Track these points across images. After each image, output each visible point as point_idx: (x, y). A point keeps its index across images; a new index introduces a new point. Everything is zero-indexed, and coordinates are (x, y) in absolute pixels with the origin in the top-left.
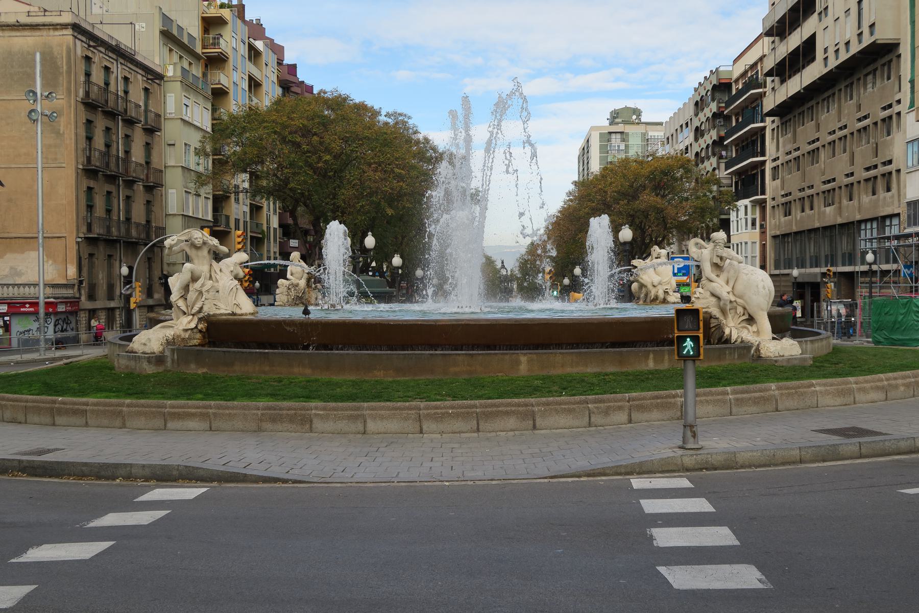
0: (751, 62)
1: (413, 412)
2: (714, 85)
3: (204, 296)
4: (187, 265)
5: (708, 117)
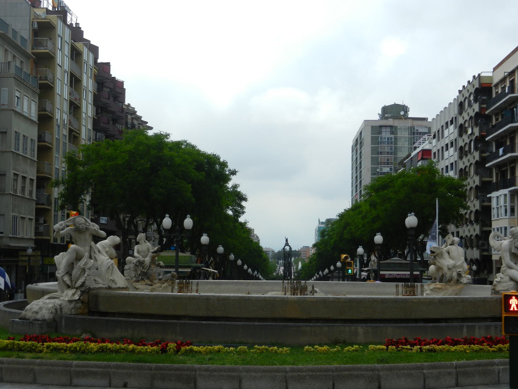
0: (510, 70)
1: (280, 374)
2: (477, 89)
3: (86, 273)
4: (72, 246)
5: (471, 116)
